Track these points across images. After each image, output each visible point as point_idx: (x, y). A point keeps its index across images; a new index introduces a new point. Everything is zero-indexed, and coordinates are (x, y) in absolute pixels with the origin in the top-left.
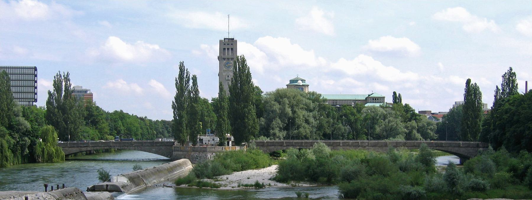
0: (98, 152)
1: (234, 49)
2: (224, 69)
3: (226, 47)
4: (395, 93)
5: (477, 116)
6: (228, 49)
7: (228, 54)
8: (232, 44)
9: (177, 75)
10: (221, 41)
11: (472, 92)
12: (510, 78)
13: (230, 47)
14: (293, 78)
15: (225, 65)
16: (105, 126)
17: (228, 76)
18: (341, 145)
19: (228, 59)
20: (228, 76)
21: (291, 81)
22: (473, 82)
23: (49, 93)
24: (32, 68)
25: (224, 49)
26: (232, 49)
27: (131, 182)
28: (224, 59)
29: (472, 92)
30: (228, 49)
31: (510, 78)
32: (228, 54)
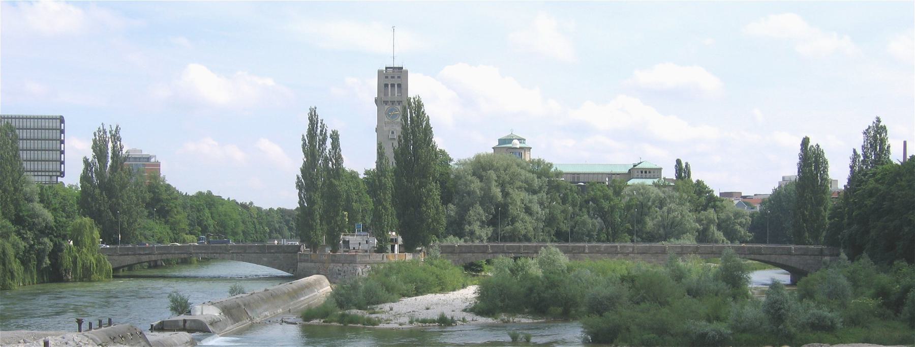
0: (168, 263)
1: (403, 86)
2: (386, 120)
3: (390, 82)
6: (393, 85)
7: (393, 94)
8: (399, 77)
10: (380, 72)
11: (812, 161)
12: (876, 137)
13: (396, 81)
14: (503, 135)
15: (387, 114)
16: (182, 218)
17: (393, 133)
18: (587, 251)
19: (393, 103)
20: (393, 133)
21: (502, 141)
22: (812, 143)
24: (56, 119)
25: (386, 85)
26: (399, 86)
28: (386, 103)
29: (812, 161)
30: (393, 85)
31: (876, 137)
32: (393, 94)
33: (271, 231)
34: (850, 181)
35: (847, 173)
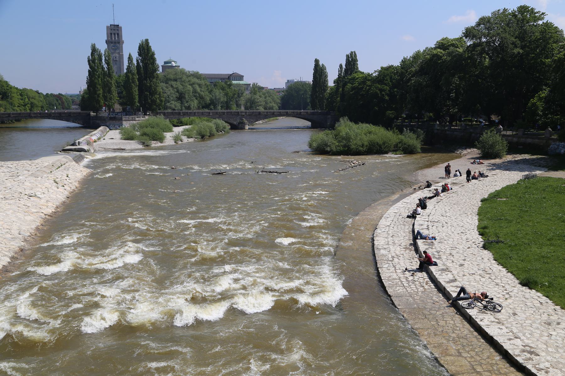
0: (30, 116)
3: (113, 32)
4: (317, 61)
5: (325, 90)
6: (114, 34)
7: (115, 38)
9: (89, 54)
10: (107, 27)
11: (319, 71)
12: (352, 61)
13: (116, 32)
14: (166, 60)
16: (16, 99)
21: (165, 63)
22: (321, 63)
23: (94, 50)
25: (111, 34)
26: (118, 34)
27: (283, 99)
28: (112, 43)
29: (319, 71)
30: (114, 34)
31: (352, 61)
32: (115, 38)
33: (226, 83)
34: (347, 291)
35: (344, 290)
